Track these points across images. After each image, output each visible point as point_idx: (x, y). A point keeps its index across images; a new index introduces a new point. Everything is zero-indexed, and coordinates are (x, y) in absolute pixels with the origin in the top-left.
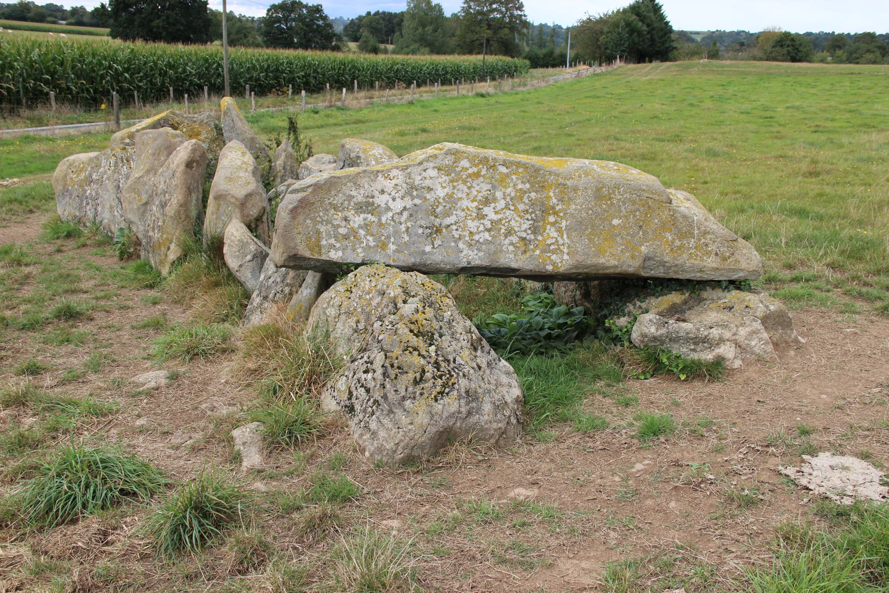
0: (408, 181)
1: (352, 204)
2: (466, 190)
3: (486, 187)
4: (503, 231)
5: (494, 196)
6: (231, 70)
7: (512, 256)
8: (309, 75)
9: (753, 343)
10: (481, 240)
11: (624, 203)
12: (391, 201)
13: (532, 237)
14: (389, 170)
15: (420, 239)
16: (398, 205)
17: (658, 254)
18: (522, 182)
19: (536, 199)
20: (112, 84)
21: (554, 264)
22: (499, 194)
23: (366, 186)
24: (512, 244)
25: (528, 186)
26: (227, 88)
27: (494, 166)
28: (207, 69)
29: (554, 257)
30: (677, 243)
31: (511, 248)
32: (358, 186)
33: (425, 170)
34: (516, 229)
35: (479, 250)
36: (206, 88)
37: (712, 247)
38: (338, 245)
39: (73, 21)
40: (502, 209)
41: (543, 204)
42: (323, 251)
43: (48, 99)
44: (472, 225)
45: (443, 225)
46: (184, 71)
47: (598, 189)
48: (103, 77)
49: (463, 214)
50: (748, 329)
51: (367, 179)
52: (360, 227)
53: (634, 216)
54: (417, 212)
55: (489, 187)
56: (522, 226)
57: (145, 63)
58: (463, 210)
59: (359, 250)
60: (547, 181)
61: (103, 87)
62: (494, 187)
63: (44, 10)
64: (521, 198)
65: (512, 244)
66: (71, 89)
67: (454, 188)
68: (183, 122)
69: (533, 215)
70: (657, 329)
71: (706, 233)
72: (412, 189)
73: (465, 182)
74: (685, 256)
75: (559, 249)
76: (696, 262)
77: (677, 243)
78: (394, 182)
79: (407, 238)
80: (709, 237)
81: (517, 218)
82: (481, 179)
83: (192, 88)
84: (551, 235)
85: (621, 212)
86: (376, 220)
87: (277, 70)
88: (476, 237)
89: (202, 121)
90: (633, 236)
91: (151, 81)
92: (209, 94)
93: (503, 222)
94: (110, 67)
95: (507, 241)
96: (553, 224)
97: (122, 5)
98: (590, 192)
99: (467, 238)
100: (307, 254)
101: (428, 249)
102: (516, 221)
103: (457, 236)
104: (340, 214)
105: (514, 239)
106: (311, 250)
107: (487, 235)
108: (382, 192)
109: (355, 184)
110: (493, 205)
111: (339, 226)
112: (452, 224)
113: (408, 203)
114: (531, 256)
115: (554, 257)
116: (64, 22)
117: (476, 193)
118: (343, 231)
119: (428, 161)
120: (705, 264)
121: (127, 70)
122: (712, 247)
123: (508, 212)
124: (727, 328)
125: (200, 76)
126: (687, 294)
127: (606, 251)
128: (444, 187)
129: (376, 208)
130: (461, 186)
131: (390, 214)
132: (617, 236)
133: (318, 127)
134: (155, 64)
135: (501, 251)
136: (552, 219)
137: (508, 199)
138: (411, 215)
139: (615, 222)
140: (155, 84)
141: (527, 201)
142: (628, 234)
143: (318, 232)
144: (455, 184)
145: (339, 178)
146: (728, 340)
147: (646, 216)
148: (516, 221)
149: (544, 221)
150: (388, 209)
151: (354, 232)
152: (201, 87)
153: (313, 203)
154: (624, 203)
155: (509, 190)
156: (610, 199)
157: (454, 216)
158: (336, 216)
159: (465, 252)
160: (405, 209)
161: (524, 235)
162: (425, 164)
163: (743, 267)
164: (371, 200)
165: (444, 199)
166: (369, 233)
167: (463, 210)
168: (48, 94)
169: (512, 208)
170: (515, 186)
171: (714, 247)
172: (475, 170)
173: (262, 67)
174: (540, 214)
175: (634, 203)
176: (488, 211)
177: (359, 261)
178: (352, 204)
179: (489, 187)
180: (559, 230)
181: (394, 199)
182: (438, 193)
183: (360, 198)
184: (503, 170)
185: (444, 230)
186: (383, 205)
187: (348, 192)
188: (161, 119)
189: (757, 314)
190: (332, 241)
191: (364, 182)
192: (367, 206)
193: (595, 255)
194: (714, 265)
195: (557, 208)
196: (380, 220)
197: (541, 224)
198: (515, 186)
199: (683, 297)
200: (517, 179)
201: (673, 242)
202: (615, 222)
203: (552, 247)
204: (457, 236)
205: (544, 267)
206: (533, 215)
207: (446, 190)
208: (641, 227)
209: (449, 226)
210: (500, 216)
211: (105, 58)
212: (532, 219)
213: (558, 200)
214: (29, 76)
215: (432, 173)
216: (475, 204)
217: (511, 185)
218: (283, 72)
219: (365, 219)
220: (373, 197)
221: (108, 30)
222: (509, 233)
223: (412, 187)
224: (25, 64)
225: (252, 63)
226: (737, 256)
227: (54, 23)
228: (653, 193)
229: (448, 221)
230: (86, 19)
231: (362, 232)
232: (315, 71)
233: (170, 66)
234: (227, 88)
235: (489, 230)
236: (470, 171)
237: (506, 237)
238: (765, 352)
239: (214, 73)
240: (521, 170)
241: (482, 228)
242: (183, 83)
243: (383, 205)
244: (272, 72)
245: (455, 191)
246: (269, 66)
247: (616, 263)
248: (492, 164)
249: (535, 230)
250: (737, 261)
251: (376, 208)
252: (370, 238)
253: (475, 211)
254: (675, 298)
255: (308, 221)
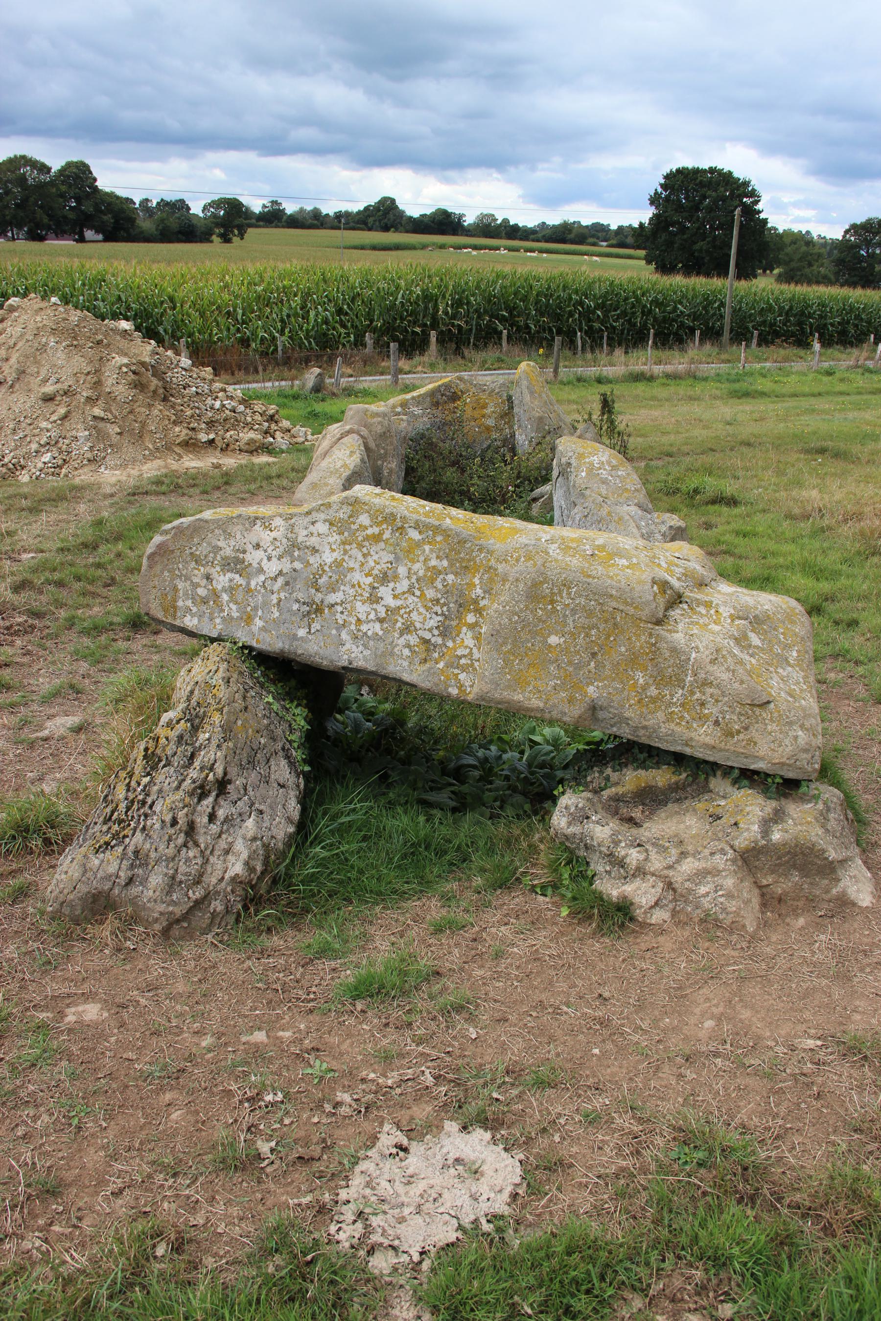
0: (289, 535)
1: (219, 558)
2: (360, 558)
3: (387, 557)
4: (399, 625)
5: (395, 572)
6: (735, 311)
7: (405, 664)
8: (848, 322)
9: (703, 890)
10: (370, 633)
11: (574, 612)
12: (265, 561)
13: (439, 641)
14: (271, 518)
15: (294, 619)
16: (272, 568)
17: (615, 704)
18: (438, 557)
19: (453, 585)
20: (581, 323)
21: (461, 687)
22: (402, 570)
23: (238, 536)
24: (408, 646)
25: (445, 563)
26: (726, 335)
27: (402, 528)
28: (704, 308)
29: (462, 676)
30: (653, 691)
31: (406, 652)
32: (228, 535)
33: (313, 523)
34: (418, 625)
35: (365, 646)
36: (698, 333)
37: (711, 710)
38: (194, 609)
39: (614, 242)
40: (404, 593)
41: (461, 594)
42: (179, 614)
43: (500, 338)
44: (362, 609)
45: (326, 603)
46: (675, 309)
47: (535, 585)
48: (571, 314)
49: (352, 592)
50: (701, 865)
51: (240, 527)
52: (224, 590)
53: (587, 635)
54: (295, 580)
55: (391, 557)
56: (427, 622)
57: (626, 299)
58: (353, 586)
59: (218, 621)
60: (474, 559)
61: (569, 326)
62: (397, 559)
63: (586, 231)
64: (432, 581)
65: (408, 646)
66: (529, 328)
67: (345, 552)
68: (468, 391)
69: (445, 609)
70: (569, 824)
71: (706, 683)
72: (293, 547)
73: (360, 546)
74: (660, 715)
75: (472, 665)
76: (678, 729)
77: (653, 691)
78: (274, 534)
79: (277, 614)
80: (710, 691)
81: (422, 610)
82: (382, 545)
83: (681, 332)
84: (466, 642)
85: (565, 624)
86: (244, 583)
87: (802, 313)
88: (364, 628)
89: (493, 391)
90: (578, 667)
91: (629, 321)
92: (701, 340)
93: (402, 611)
94: (581, 303)
95: (402, 641)
96: (472, 627)
97: (663, 224)
98: (521, 586)
99: (353, 627)
100: (160, 615)
101: (302, 633)
102: (420, 614)
103: (341, 622)
104: (202, 569)
105: (413, 640)
106: (166, 611)
107: (377, 626)
108: (257, 546)
109: (224, 531)
110: (391, 585)
111: (197, 585)
112: (337, 604)
113: (286, 565)
114: (430, 668)
115: (462, 676)
116: (605, 244)
117: (373, 564)
118: (202, 592)
119: (318, 510)
120: (693, 735)
121: (598, 307)
122: (711, 710)
123: (411, 599)
124: (676, 856)
125: (695, 317)
126: (684, 775)
127: (529, 684)
128: (333, 550)
129: (247, 567)
130: (355, 552)
131: (262, 578)
132: (551, 662)
133: (813, 395)
134: (638, 300)
135: (392, 654)
136: (471, 618)
137: (414, 580)
138: (287, 583)
139: (553, 640)
140: (635, 325)
141: (440, 586)
142: (570, 663)
143: (175, 589)
144: (348, 547)
145: (206, 521)
146: (653, 875)
147: (608, 636)
148: (420, 614)
149: (460, 620)
150: (261, 570)
151: (215, 595)
152: (692, 331)
153: (173, 552)
154: (574, 612)
155: (417, 566)
156: (552, 602)
157: (341, 593)
158: (196, 572)
159: (348, 646)
160: (280, 573)
161: (428, 636)
162: (314, 514)
163: (761, 753)
164: (241, 556)
165: (330, 567)
166: (233, 600)
167: (353, 586)
168: (501, 332)
169: (418, 593)
170: (426, 560)
171: (715, 710)
172: (376, 530)
173: (781, 308)
174: (457, 608)
175: (590, 614)
176: (384, 592)
177: (214, 634)
178: (219, 558)
179: (391, 557)
180: (477, 638)
181: (269, 559)
182: (324, 558)
183: (228, 552)
184: (414, 535)
185: (326, 611)
186: (255, 565)
187: (215, 542)
188: (443, 385)
189: (736, 843)
190: (189, 603)
191: (237, 530)
192: (236, 564)
193: (508, 687)
194: (708, 740)
195: (482, 603)
196: (248, 584)
197: (454, 623)
198: (426, 560)
199: (674, 779)
200: (431, 551)
201: (645, 688)
202: (553, 640)
203: (463, 661)
204: (341, 622)
205: (446, 689)
206: (445, 609)
207: (335, 555)
208: (594, 655)
209: (333, 606)
210: (399, 603)
211: (576, 292)
212: (443, 614)
213: (485, 592)
214: (486, 311)
215: (322, 528)
216: (370, 580)
217: (422, 558)
218: (810, 316)
219: (231, 580)
220: (244, 552)
221: (642, 253)
222: (408, 629)
223: (294, 545)
224: (484, 298)
225: (768, 302)
226: (753, 733)
227: (594, 244)
228: (626, 603)
229: (332, 598)
230: (630, 240)
231: (225, 597)
232: (858, 317)
233: (656, 302)
234: (726, 335)
235: (381, 621)
236: (370, 531)
237: (401, 635)
238: (724, 910)
239: (714, 314)
240: (439, 538)
241: (372, 616)
242: (671, 325)
243: (255, 565)
244: (795, 316)
245: (346, 558)
246: (791, 308)
247: (541, 705)
248: (400, 524)
249: (445, 631)
250: (752, 742)
251: (247, 567)
252: (234, 607)
253: (368, 589)
254: (661, 777)
255: (166, 574)
